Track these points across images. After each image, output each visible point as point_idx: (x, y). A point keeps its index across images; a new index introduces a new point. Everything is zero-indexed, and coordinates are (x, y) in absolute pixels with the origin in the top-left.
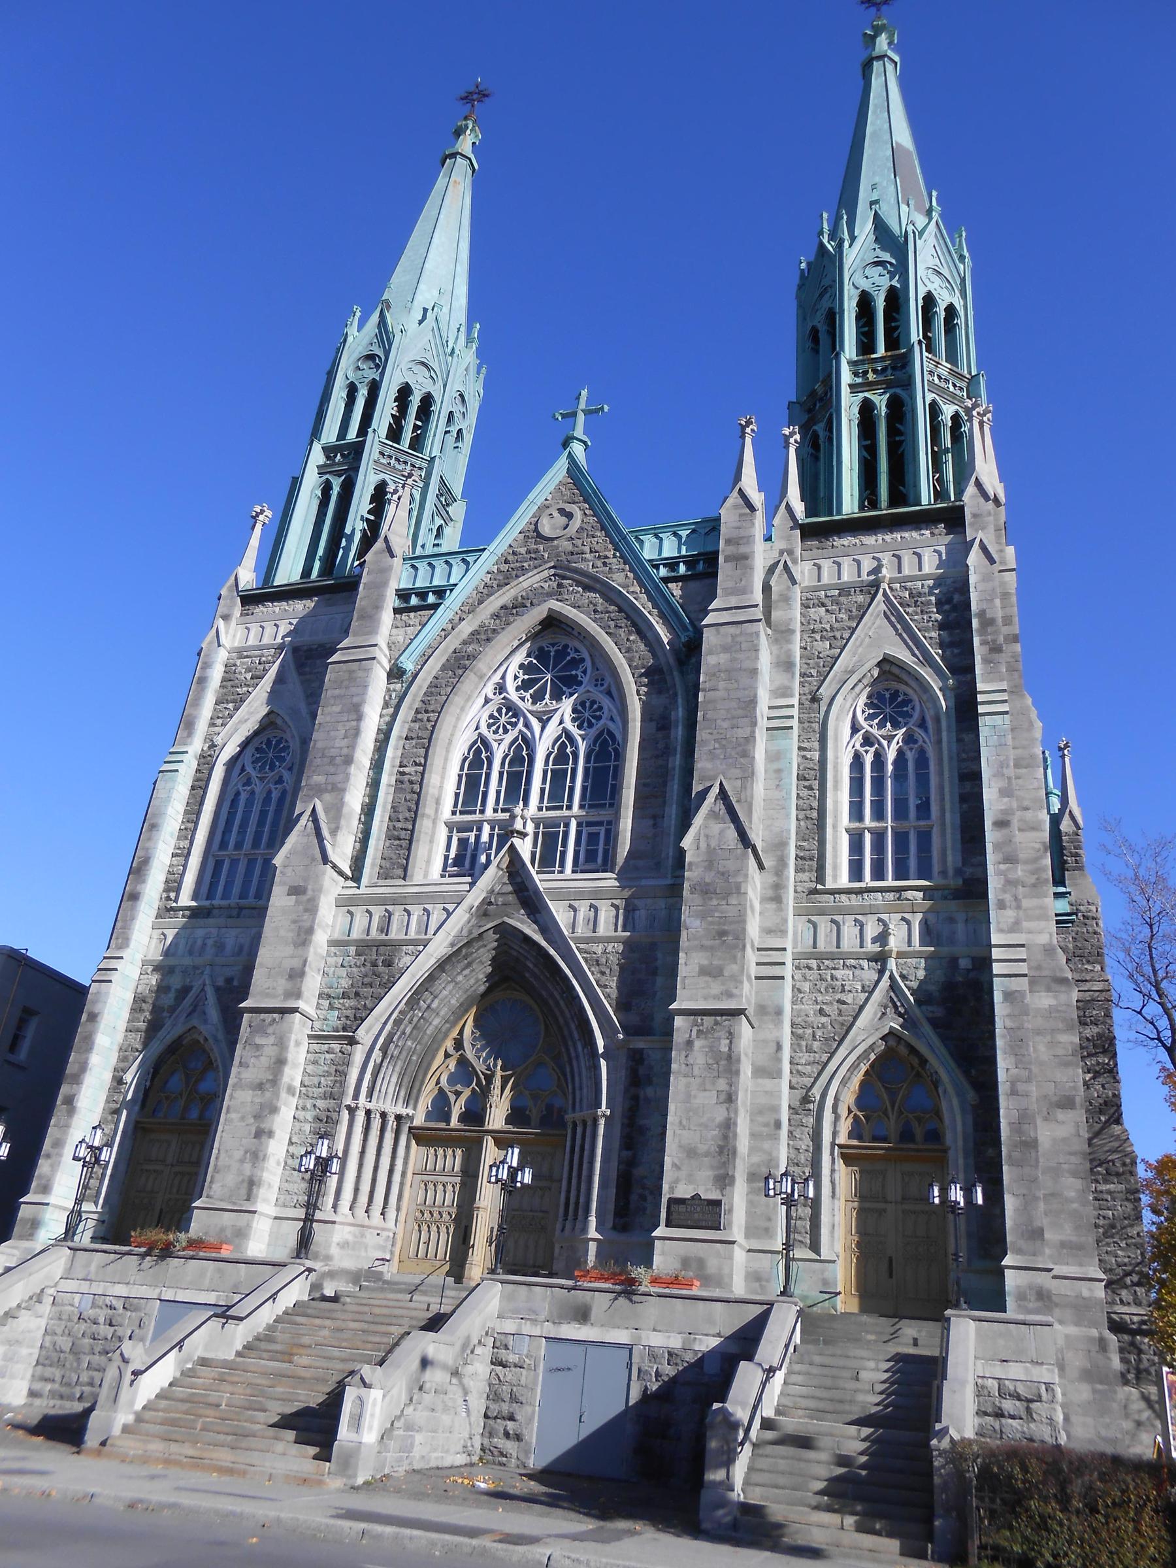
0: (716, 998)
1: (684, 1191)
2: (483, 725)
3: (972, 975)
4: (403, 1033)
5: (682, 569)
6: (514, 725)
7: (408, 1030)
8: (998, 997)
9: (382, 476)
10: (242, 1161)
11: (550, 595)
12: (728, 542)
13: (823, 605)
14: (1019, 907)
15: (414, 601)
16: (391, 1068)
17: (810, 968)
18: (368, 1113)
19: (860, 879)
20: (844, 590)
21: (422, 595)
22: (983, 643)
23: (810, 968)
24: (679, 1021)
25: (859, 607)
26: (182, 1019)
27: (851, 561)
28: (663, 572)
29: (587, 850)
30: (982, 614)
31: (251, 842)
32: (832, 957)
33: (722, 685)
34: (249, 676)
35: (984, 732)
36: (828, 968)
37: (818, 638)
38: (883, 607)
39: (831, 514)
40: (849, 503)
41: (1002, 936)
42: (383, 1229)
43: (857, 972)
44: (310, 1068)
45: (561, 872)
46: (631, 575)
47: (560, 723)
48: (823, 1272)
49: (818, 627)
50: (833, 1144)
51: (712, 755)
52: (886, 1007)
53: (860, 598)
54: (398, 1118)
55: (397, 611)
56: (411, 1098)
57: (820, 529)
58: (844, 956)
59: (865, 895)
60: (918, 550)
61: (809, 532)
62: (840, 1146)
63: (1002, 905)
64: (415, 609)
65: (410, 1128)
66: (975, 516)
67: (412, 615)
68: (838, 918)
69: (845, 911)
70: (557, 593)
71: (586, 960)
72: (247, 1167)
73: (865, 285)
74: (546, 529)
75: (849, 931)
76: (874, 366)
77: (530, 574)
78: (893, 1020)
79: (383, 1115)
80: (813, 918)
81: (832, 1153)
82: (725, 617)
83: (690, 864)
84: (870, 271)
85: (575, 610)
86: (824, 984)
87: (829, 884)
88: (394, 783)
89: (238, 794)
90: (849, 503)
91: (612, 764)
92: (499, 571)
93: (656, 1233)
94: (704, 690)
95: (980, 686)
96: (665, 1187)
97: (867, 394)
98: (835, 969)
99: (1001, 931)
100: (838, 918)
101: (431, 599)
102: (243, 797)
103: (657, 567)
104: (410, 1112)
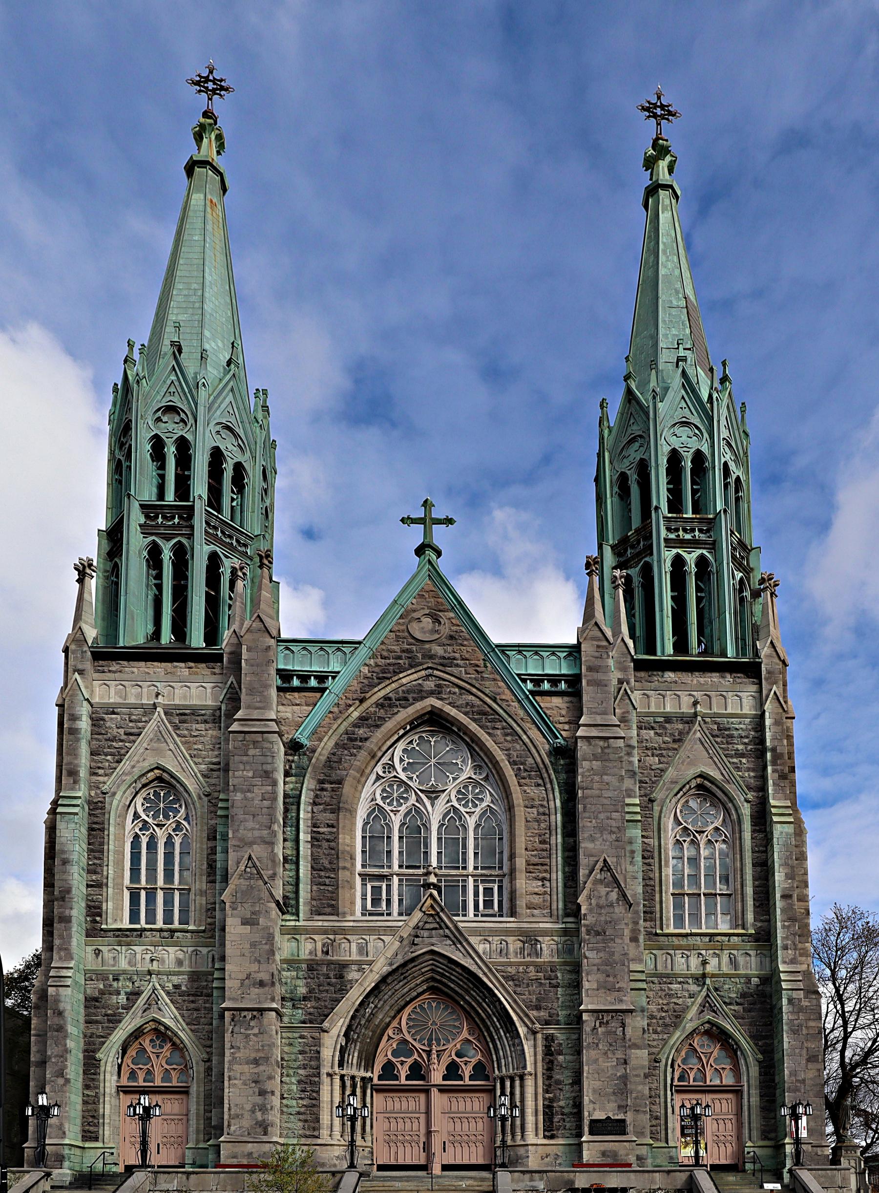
0: (611, 1003)
1: (599, 1115)
2: (378, 797)
3: (760, 988)
4: (359, 1024)
5: (563, 686)
6: (406, 799)
7: (363, 1022)
8: (785, 1001)
9: (212, 547)
10: (253, 1111)
11: (431, 693)
12: (590, 669)
13: (653, 728)
14: (795, 949)
15: (296, 682)
16: (353, 1046)
17: (653, 983)
18: (342, 1077)
19: (683, 927)
20: (668, 719)
21: (304, 678)
22: (774, 771)
23: (653, 983)
24: (585, 1017)
25: (680, 733)
26: (140, 1014)
27: (676, 696)
28: (530, 686)
29: (484, 901)
30: (774, 750)
31: (129, 878)
32: (668, 976)
33: (596, 786)
34: (122, 731)
35: (776, 835)
36: (665, 983)
37: (650, 754)
38: (698, 735)
39: (655, 654)
40: (666, 647)
41: (785, 966)
42: (366, 1147)
43: (685, 986)
44: (286, 1049)
45: (465, 915)
46: (501, 684)
47: (448, 802)
48: (669, 1153)
49: (649, 745)
50: (672, 1085)
51: (592, 839)
52: (704, 1007)
53: (680, 726)
54: (363, 1079)
55: (279, 689)
56: (369, 1065)
57: (648, 667)
58: (676, 976)
59: (689, 938)
60: (724, 693)
61: (640, 666)
62: (676, 1086)
63: (785, 948)
64: (313, 690)
65: (372, 1085)
66: (769, 672)
67: (296, 694)
68: (672, 952)
69: (676, 948)
70: (437, 693)
71: (502, 976)
72: (259, 1116)
73: (676, 443)
74: (416, 630)
75: (680, 961)
76: (684, 525)
77: (409, 672)
78: (708, 1014)
79: (353, 1078)
80: (654, 952)
81: (671, 1090)
82: (594, 732)
83: (585, 915)
84: (679, 430)
85: (454, 710)
86: (664, 993)
87: (666, 931)
88: (309, 839)
89: (136, 837)
90: (666, 647)
91: (461, 837)
92: (377, 665)
93: (583, 1139)
94: (583, 789)
95: (773, 802)
96: (586, 1114)
97: (680, 551)
98: (670, 983)
99: (784, 962)
100: (672, 952)
101: (313, 683)
102: (144, 841)
103: (524, 681)
104: (369, 1074)
